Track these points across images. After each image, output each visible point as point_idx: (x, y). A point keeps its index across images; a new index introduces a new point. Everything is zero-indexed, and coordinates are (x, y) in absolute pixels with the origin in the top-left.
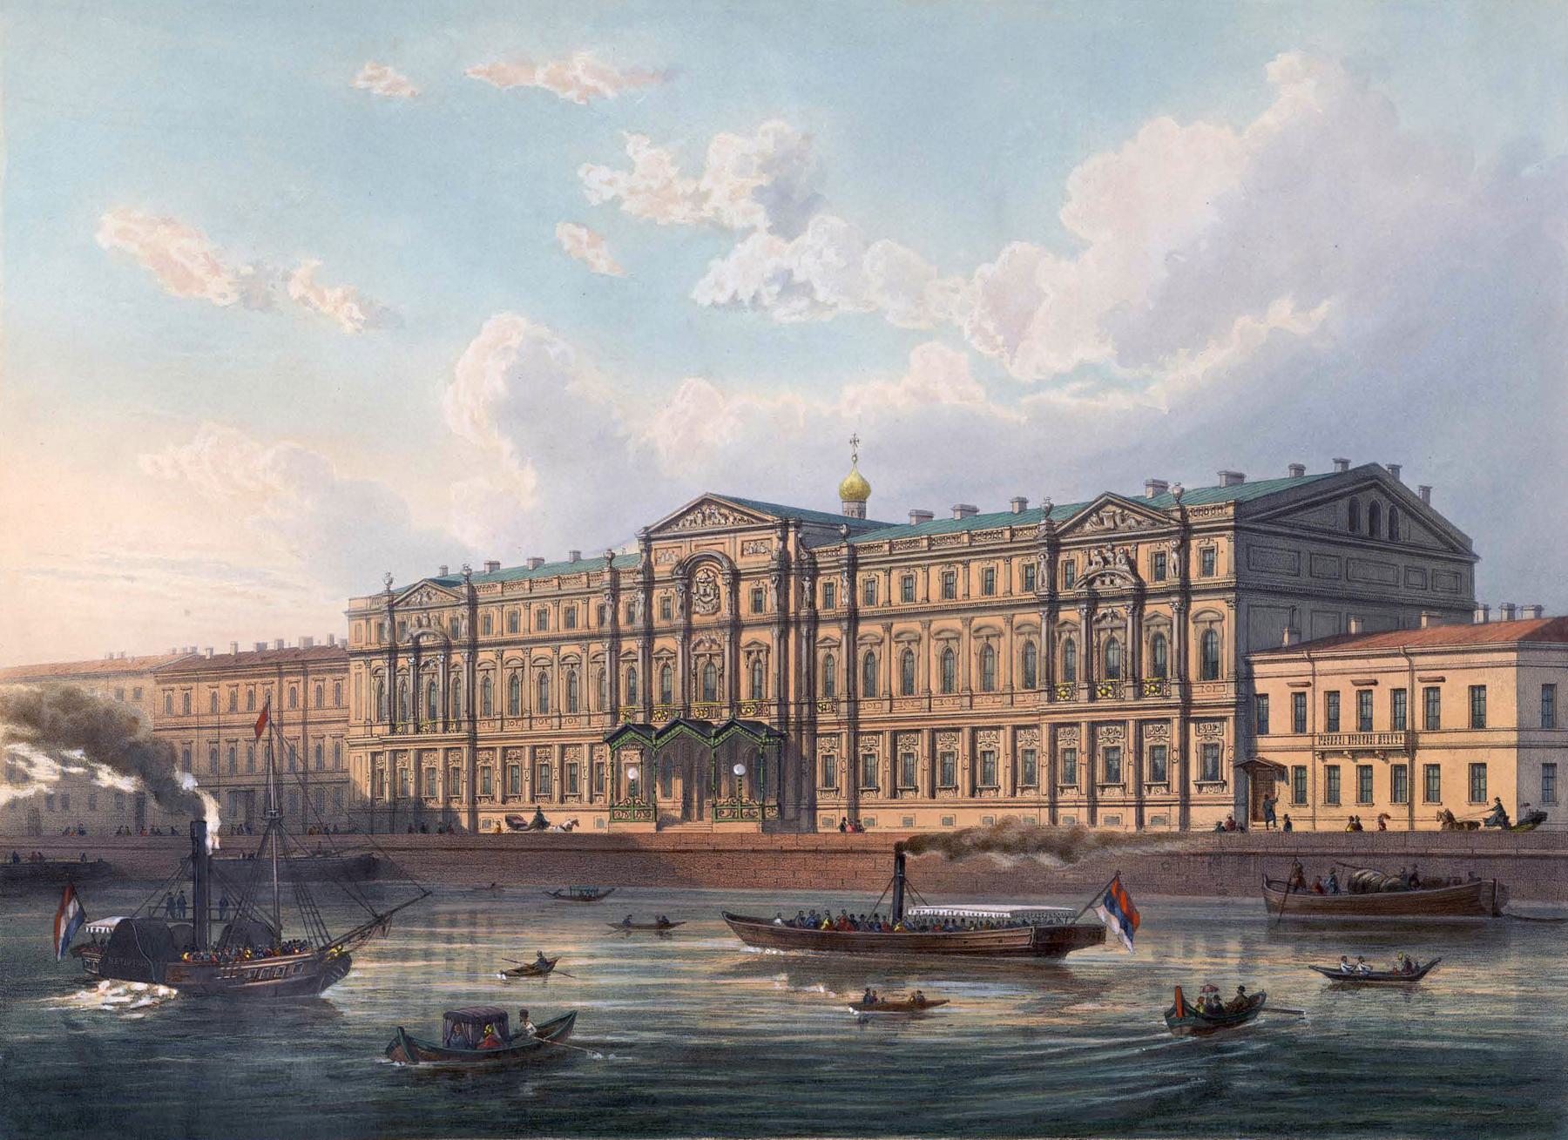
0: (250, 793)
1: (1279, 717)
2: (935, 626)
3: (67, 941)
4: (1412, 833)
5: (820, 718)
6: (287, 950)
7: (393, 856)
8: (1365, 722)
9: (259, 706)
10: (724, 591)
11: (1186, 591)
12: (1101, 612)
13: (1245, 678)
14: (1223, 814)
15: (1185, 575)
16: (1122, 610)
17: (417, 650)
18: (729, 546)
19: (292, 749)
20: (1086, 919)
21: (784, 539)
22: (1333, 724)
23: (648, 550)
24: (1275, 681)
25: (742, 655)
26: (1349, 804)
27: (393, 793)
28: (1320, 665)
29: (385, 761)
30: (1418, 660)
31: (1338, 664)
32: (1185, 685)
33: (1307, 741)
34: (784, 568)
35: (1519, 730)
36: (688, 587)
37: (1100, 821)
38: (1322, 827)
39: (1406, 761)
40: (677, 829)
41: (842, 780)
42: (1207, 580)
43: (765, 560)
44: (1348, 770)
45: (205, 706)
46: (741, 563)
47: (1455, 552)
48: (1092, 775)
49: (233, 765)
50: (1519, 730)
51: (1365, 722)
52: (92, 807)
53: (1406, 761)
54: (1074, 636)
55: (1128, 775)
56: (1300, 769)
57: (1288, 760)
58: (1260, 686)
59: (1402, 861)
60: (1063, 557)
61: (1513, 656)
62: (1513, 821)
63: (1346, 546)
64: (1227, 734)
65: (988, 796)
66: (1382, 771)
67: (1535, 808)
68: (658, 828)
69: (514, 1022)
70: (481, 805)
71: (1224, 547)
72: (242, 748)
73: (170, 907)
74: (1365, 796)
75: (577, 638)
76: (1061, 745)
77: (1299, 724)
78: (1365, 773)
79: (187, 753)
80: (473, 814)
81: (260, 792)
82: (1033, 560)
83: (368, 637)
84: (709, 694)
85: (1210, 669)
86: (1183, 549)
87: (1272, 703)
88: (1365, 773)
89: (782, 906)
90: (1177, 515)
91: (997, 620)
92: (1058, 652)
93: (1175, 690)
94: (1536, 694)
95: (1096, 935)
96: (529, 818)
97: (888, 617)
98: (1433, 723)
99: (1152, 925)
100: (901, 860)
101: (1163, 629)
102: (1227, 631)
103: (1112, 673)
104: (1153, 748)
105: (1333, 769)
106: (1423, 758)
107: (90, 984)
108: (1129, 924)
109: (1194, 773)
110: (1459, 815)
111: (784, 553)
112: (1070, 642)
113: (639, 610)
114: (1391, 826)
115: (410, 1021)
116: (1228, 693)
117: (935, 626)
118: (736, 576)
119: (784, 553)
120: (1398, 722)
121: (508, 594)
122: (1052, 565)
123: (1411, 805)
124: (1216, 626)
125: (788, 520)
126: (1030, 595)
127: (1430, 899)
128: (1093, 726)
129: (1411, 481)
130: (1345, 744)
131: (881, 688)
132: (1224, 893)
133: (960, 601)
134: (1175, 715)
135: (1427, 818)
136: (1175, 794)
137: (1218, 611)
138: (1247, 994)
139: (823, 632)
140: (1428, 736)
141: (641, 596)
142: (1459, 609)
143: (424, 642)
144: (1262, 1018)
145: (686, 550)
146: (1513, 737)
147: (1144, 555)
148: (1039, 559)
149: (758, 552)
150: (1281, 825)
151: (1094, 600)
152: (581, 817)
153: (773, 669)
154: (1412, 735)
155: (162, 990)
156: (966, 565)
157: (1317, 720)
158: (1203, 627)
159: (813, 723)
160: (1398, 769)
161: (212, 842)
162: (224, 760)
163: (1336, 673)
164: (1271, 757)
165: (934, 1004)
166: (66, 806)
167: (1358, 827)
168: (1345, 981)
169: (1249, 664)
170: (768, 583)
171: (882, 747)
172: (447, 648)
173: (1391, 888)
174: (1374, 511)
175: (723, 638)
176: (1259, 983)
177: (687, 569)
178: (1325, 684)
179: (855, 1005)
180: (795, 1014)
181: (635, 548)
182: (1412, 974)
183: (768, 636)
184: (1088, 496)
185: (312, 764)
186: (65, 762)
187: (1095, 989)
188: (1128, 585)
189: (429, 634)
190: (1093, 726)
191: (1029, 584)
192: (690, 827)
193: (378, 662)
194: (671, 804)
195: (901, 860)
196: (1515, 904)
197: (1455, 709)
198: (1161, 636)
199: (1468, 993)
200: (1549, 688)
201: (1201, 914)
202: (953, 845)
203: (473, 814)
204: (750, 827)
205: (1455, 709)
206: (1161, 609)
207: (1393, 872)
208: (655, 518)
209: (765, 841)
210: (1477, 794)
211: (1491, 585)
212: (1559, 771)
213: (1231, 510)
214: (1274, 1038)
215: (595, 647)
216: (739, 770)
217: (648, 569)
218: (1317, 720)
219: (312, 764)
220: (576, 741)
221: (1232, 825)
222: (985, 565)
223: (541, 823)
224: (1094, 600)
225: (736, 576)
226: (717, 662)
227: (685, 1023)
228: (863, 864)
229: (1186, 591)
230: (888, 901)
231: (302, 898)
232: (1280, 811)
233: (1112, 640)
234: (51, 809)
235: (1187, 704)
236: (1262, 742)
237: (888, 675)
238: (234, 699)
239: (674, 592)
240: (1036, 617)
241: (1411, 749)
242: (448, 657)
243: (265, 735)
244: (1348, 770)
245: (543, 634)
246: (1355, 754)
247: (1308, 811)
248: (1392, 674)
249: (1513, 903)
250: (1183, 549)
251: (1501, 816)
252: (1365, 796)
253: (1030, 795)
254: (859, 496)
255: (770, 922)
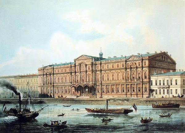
0: (26, 93)
1: (154, 83)
2: (116, 71)
3: (4, 111)
4: (155, 99)
5: (97, 83)
6: (30, 112)
7: (44, 101)
8: (164, 84)
9: (27, 82)
10: (85, 67)
11: (142, 67)
12: (132, 70)
13: (150, 78)
14: (147, 96)
15: (75, 71)
16: (135, 69)
17: (47, 74)
18: (85, 61)
19: (31, 87)
20: (131, 109)
21: (92, 60)
22: (160, 84)
23: (75, 62)
24: (153, 79)
25: (87, 75)
26: (162, 95)
27: (44, 93)
28: (158, 77)
29: (42, 89)
30: (170, 77)
31: (161, 77)
32: (143, 79)
33: (157, 86)
34: (92, 64)
35: (181, 85)
36: (80, 66)
37: (132, 97)
38: (159, 97)
39: (168, 89)
40: (79, 97)
41: (100, 91)
42: (103, 69)
43: (90, 63)
44: (162, 90)
45: (21, 82)
46: (87, 63)
47: (174, 63)
48: (131, 91)
49: (24, 89)
50: (181, 85)
51: (164, 84)
52: (7, 94)
53: (168, 89)
54: (129, 73)
55: (135, 91)
56: (156, 90)
57: (155, 89)
58: (151, 80)
59: (168, 101)
60: (127, 63)
61: (180, 76)
62: (180, 96)
63: (161, 62)
64: (147, 86)
65: (118, 93)
66: (166, 90)
67: (183, 95)
68: (77, 97)
69: (59, 122)
70: (103, 94)
71: (147, 62)
72: (25, 87)
73: (16, 107)
74: (164, 93)
75: (63, 73)
76: (127, 87)
77: (156, 84)
78: (164, 90)
79: (18, 88)
80: (54, 95)
81: (27, 93)
82: (124, 63)
83: (41, 73)
84: (83, 80)
85: (146, 77)
86: (142, 62)
87: (153, 81)
88: (164, 90)
89: (93, 107)
90: (141, 58)
91: (119, 71)
92: (97, 77)
93: (141, 80)
94: (183, 80)
95: (131, 111)
96: (61, 96)
97: (105, 70)
98: (171, 84)
99: (139, 110)
100: (107, 102)
101: (140, 72)
102: (147, 72)
103: (133, 78)
104: (139, 87)
105: (160, 90)
106: (170, 88)
107: (7, 116)
108: (136, 109)
109: (144, 91)
110: (174, 96)
111: (92, 62)
112: (128, 74)
113: (70, 70)
114: (167, 97)
115: (46, 122)
116: (148, 80)
117: (106, 72)
118: (86, 65)
119: (92, 62)
120: (168, 84)
121: (58, 67)
122: (126, 64)
123: (169, 94)
124: (146, 72)
125: (92, 58)
126: (123, 68)
127: (171, 106)
128: (131, 84)
129: (169, 54)
130: (162, 87)
131: (104, 80)
132: (147, 106)
133: (119, 68)
134: (141, 83)
135: (171, 96)
136: (141, 93)
137: (146, 70)
138: (150, 118)
139: (97, 72)
140: (166, 86)
141: (74, 68)
142: (174, 70)
143: (48, 74)
144: (152, 121)
145: (80, 62)
146: (180, 86)
147: (137, 62)
148: (124, 63)
149: (89, 62)
150: (154, 97)
151: (131, 68)
152: (67, 96)
153: (91, 77)
154: (169, 86)
155: (16, 117)
156: (115, 64)
157: (158, 84)
158: (144, 72)
159: (96, 84)
160: (168, 90)
161: (22, 99)
162: (23, 89)
163: (160, 78)
164: (152, 88)
165: (112, 120)
166: (4, 94)
167: (163, 97)
168: (162, 116)
169: (150, 77)
170: (90, 66)
171: (104, 87)
172: (50, 74)
173: (167, 105)
174: (165, 57)
175: (85, 73)
176: (152, 117)
177: (80, 64)
178: (159, 79)
179: (102, 120)
180: (94, 121)
181: (74, 61)
182: (169, 116)
183: (90, 73)
184: (131, 55)
185: (34, 89)
186: (4, 89)
187: (132, 117)
188: (136, 66)
189: (48, 72)
190: (131, 84)
191: (123, 66)
192: (81, 97)
193: (42, 76)
194: (79, 95)
195: (107, 102)
196: (181, 107)
197: (174, 83)
198: (139, 73)
199: (176, 117)
200: (184, 80)
201: (145, 108)
202: (114, 100)
203: (54, 95)
204: (89, 97)
205: (174, 83)
206: (140, 70)
207: (167, 103)
208: (76, 58)
209: (90, 99)
210: (176, 93)
211: (178, 67)
212: (172, 90)
213: (148, 57)
214: (154, 124)
215: (69, 74)
216: (87, 90)
217: (75, 64)
218: (158, 84)
219: (34, 89)
220: (128, 83)
221: (148, 97)
222: (107, 65)
223: (62, 96)
224: (131, 68)
225: (86, 65)
226: (84, 76)
227: (80, 122)
228: (103, 102)
229: (75, 72)
230: (106, 107)
231: (33, 105)
232: (154, 95)
233: (134, 74)
234: (2, 94)
235: (143, 82)
236: (151, 87)
237: (106, 78)
238: (24, 81)
239: (78, 67)
240: (124, 70)
241: (169, 87)
242: (50, 75)
243: (28, 85)
244: (162, 90)
245: (62, 73)
246: (163, 88)
247: (157, 95)
248: (167, 78)
249: (180, 106)
250: (142, 62)
251: (179, 96)
252: (164, 93)
253: (123, 93)
254: (101, 55)
255: (91, 109)
